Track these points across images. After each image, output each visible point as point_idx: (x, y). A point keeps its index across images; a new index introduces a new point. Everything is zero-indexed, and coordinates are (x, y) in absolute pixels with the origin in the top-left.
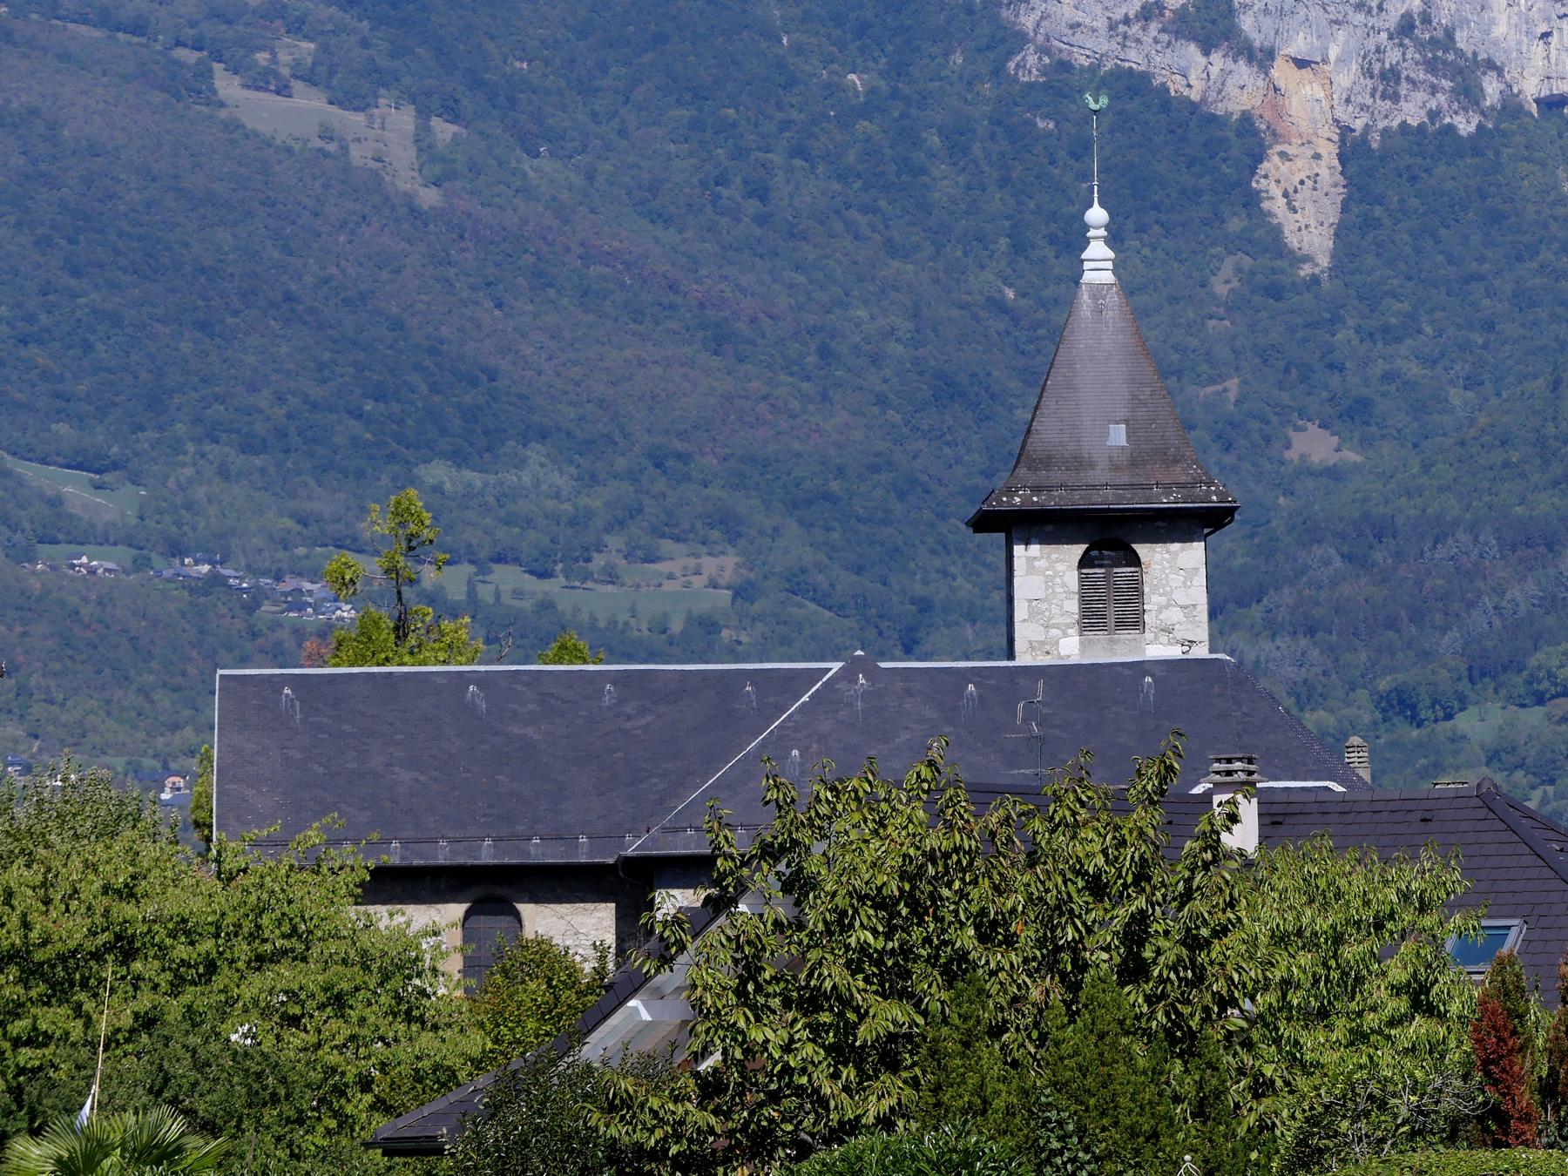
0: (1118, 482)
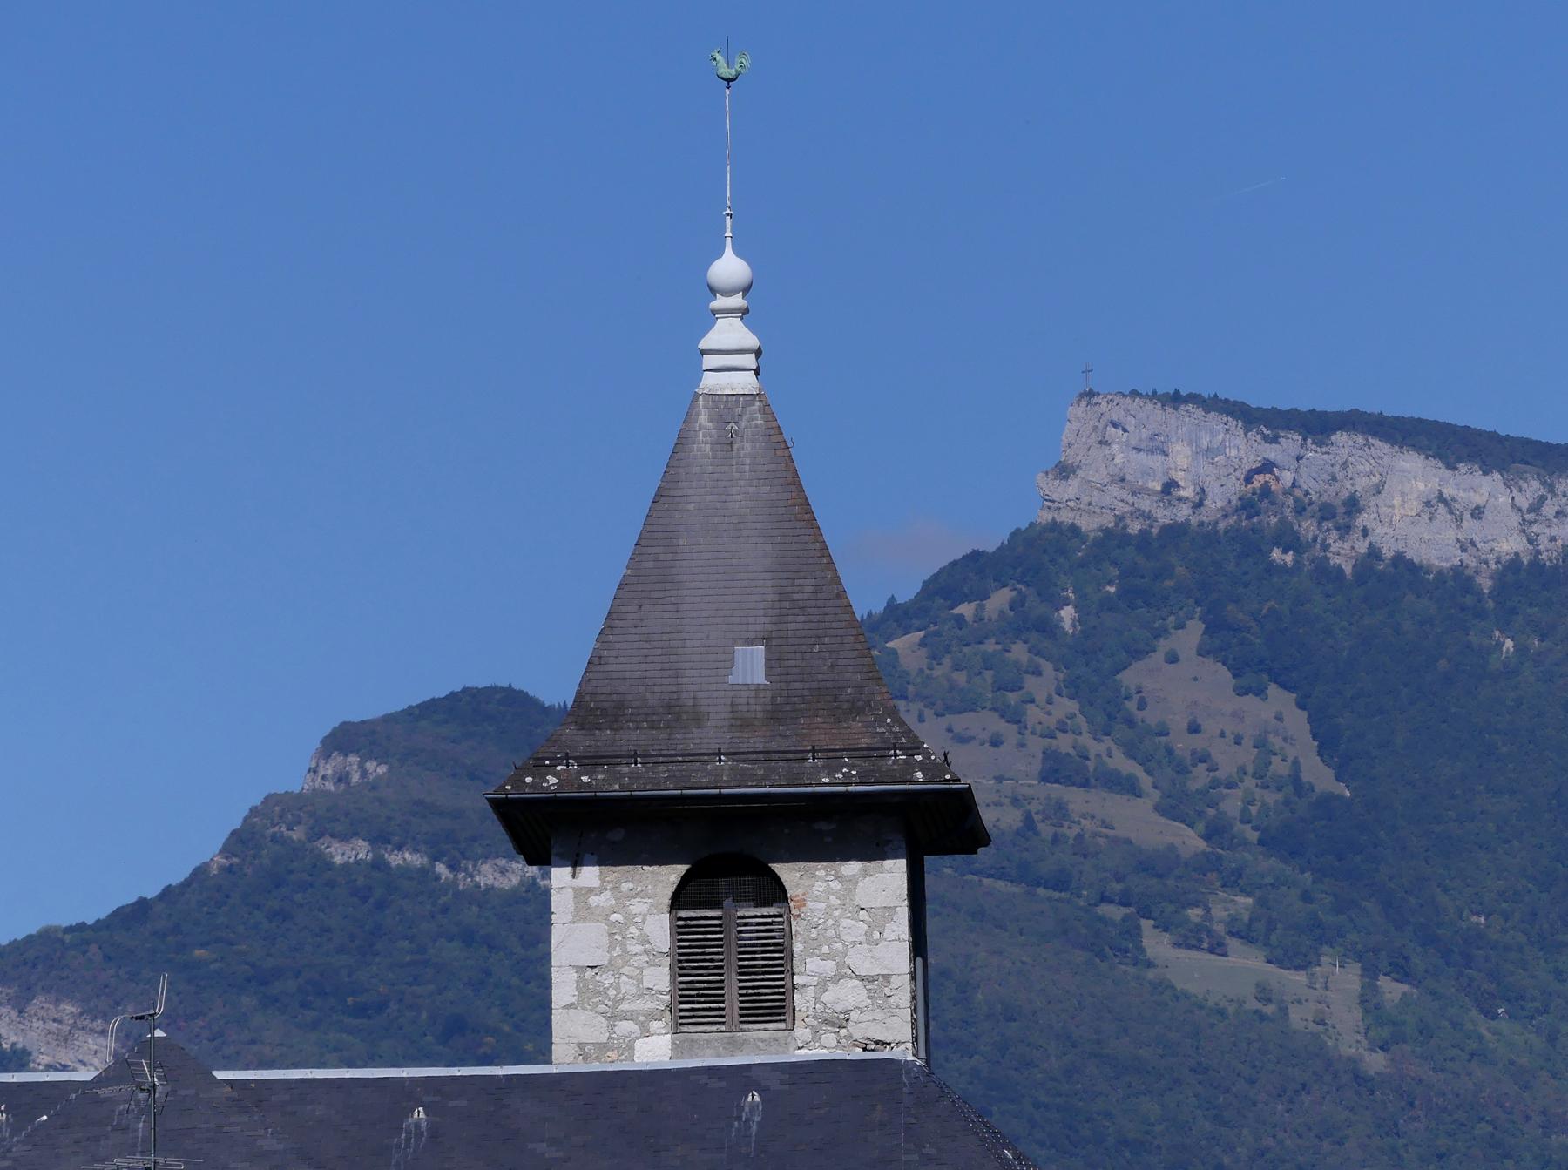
0: (744, 747)
